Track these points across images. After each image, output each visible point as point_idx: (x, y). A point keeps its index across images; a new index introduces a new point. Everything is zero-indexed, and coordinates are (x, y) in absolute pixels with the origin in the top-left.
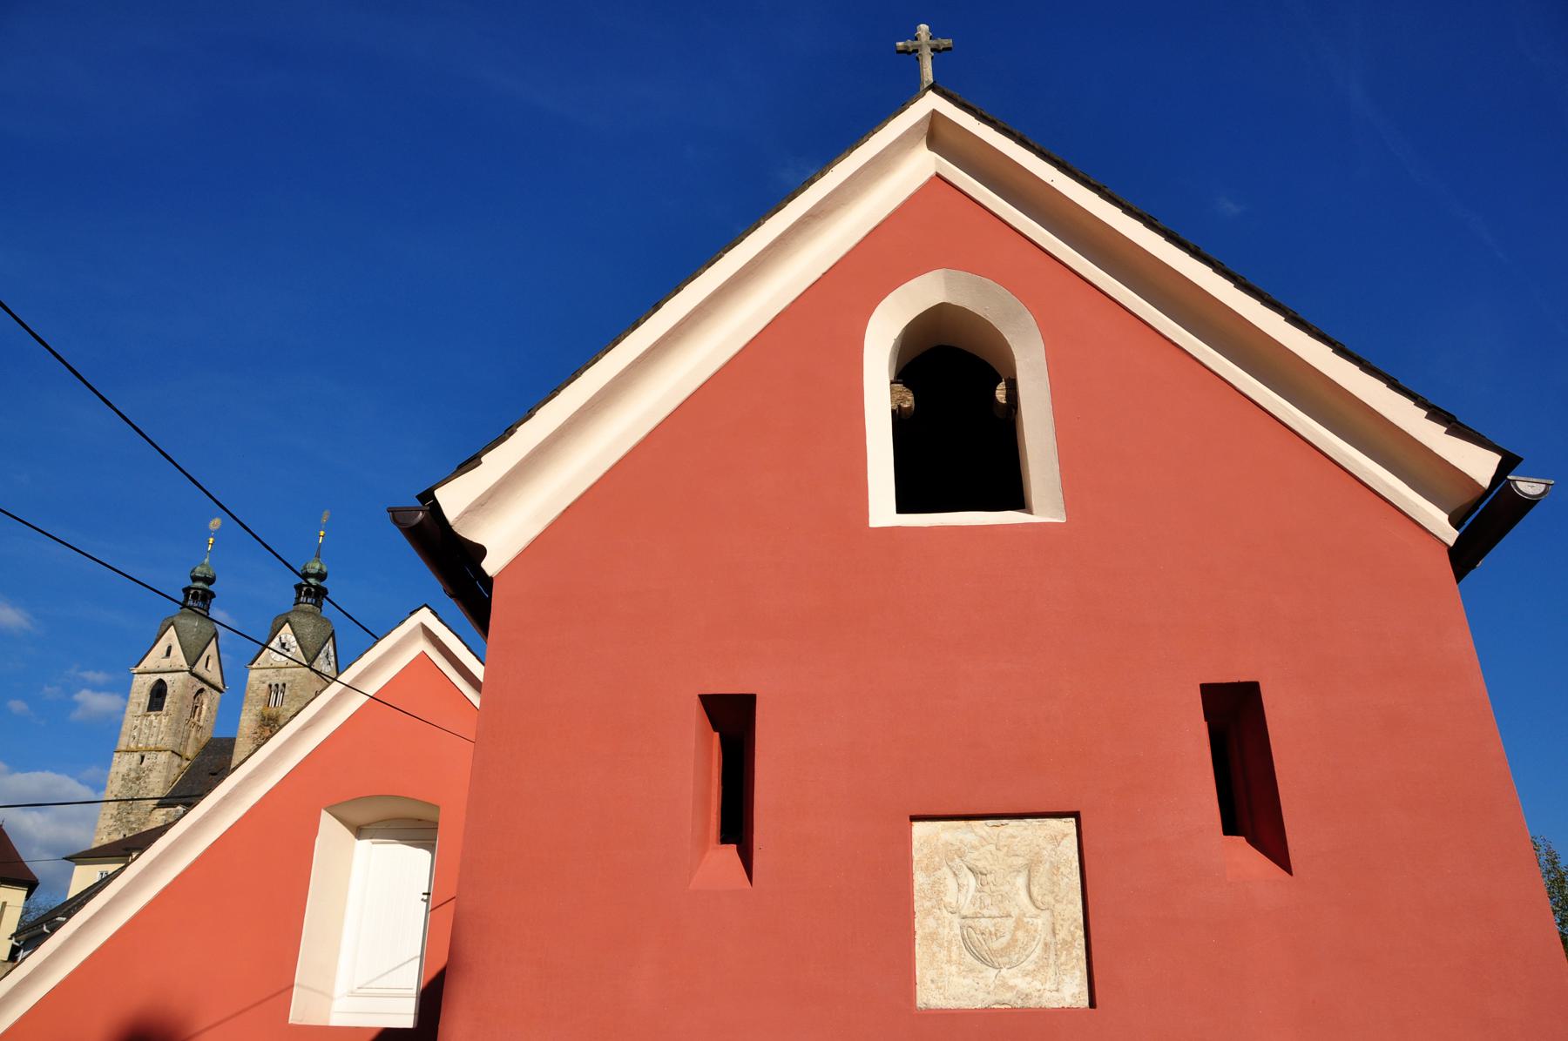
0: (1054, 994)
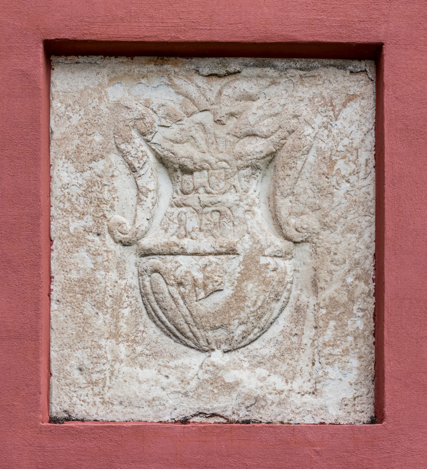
0: (308, 398)
